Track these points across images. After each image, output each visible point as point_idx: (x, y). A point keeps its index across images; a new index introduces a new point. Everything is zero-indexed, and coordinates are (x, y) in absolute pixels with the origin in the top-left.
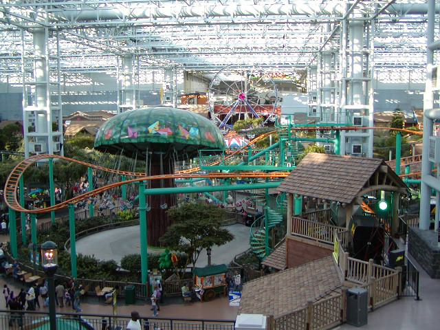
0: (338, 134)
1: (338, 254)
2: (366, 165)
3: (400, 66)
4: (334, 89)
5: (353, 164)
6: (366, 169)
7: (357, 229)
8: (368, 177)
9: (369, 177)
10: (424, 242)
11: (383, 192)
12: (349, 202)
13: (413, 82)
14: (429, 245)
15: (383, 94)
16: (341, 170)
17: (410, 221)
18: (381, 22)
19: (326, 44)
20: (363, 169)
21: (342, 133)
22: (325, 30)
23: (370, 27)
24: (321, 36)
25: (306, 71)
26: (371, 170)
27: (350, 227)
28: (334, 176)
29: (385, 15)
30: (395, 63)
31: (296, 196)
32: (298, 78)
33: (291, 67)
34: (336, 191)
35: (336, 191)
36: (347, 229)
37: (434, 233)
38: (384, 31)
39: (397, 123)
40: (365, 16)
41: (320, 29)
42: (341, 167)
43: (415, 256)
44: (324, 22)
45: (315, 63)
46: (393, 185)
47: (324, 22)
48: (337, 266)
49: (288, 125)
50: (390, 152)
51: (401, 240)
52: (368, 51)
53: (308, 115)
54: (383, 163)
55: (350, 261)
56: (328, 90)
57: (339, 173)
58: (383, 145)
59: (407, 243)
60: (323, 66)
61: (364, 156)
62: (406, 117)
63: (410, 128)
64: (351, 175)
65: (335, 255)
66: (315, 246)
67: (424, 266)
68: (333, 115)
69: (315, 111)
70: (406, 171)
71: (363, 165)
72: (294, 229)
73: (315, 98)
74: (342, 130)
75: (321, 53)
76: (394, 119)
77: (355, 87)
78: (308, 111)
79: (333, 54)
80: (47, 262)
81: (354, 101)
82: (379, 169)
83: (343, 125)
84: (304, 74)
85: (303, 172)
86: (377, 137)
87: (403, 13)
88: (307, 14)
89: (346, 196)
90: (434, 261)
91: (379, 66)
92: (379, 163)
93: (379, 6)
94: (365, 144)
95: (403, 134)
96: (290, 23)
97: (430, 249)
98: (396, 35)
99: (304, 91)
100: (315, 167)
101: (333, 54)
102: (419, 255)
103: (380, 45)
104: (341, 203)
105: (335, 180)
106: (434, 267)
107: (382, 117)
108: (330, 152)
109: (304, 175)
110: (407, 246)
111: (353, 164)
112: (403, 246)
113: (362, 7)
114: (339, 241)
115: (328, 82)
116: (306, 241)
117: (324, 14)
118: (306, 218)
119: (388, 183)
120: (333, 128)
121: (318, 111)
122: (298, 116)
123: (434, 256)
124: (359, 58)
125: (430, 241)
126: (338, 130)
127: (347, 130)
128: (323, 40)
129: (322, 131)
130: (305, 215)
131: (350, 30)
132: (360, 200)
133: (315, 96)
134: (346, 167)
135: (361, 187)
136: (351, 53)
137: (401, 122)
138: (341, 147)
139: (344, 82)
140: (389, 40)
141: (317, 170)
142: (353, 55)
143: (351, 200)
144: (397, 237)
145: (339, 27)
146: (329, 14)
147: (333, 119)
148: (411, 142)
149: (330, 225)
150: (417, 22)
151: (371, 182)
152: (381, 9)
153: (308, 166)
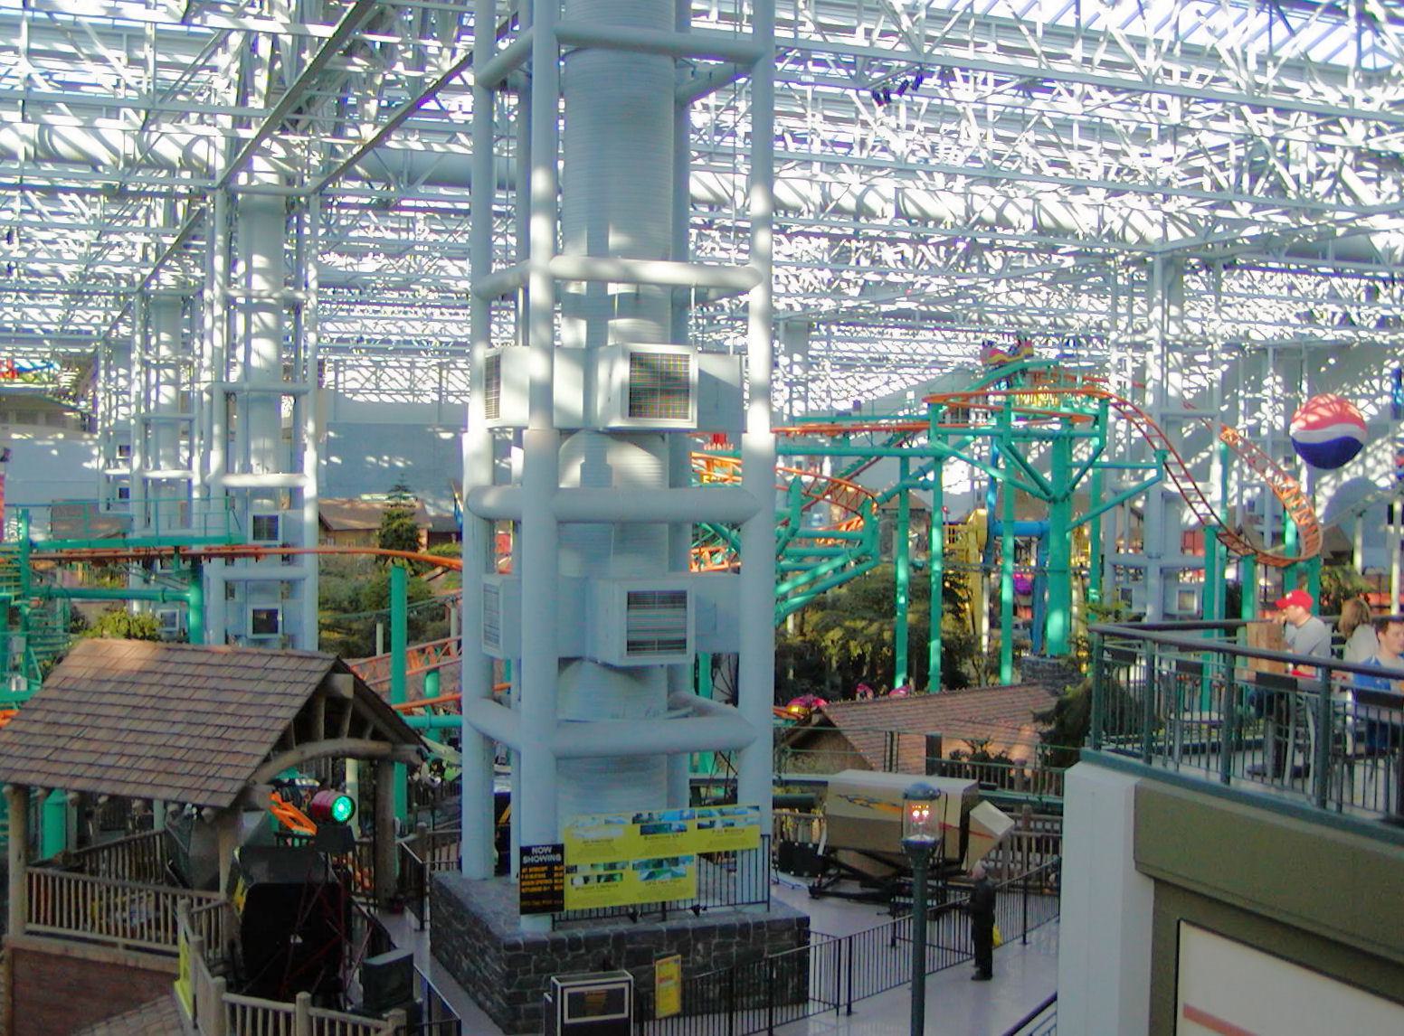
0: (196, 573)
1: (195, 987)
2: (284, 676)
3: (407, 348)
4: (191, 421)
5: (239, 673)
6: (281, 688)
7: (255, 894)
8: (288, 714)
9: (294, 712)
10: (477, 920)
11: (351, 766)
12: (225, 802)
13: (451, 399)
14: (496, 931)
15: (355, 434)
16: (199, 695)
17: (444, 850)
18: (341, 206)
19: (161, 265)
20: (272, 688)
21: (214, 571)
22: (158, 220)
23: (307, 218)
24: (147, 240)
25: (94, 358)
26: (299, 689)
27: (231, 889)
28: (171, 717)
29: (357, 184)
30: (394, 338)
31: (40, 792)
32: (66, 379)
33: (39, 341)
34: (180, 768)
35: (180, 768)
36: (221, 895)
37: (508, 884)
38: (353, 234)
39: (399, 536)
40: (290, 181)
41: (141, 213)
42: (199, 683)
43: (451, 967)
44: (153, 195)
45: (124, 330)
46: (376, 736)
47: (153, 195)
48: (189, 1027)
49: (20, 544)
50: (380, 629)
51: (410, 918)
52: (300, 295)
53: (102, 508)
54: (338, 667)
55: (233, 1007)
56: (171, 424)
57: (191, 706)
58: (355, 604)
59: (427, 926)
60: (153, 341)
61: (290, 640)
62: (432, 512)
63: (445, 547)
64: (230, 709)
65: (182, 989)
66: (114, 965)
67: (481, 997)
68: (187, 506)
69: (124, 493)
70: (430, 684)
71: (272, 676)
72: (33, 914)
73: (125, 450)
74: (209, 556)
75: (145, 296)
76: (391, 517)
77: (257, 414)
78: (101, 494)
79: (186, 302)
80: (916, 831)
81: (253, 461)
82: (324, 687)
83: (216, 540)
84: (87, 368)
85: (62, 707)
86: (335, 581)
87: (412, 181)
88: (93, 163)
89: (213, 785)
90: (509, 977)
91: (341, 346)
92: (326, 666)
93: (332, 150)
94: (290, 604)
95: (418, 567)
96: (33, 189)
97: (495, 940)
98: (394, 250)
99: (87, 424)
100: (107, 687)
101: (185, 299)
102: (465, 963)
103: (341, 279)
104: (200, 808)
105: (177, 728)
106: (508, 998)
107: (355, 513)
108: (175, 637)
109: (66, 719)
110: (427, 934)
111: (239, 673)
112: (410, 939)
113: (279, 152)
114: (194, 938)
115: (167, 394)
116: (78, 951)
117: (150, 165)
118: (80, 870)
119: (356, 732)
120: (178, 553)
121: (135, 494)
122: (61, 512)
123: (510, 962)
124: (268, 318)
125: (497, 914)
126: (196, 560)
127: (230, 558)
128: (152, 257)
129: (147, 562)
130: (80, 858)
131: (241, 226)
132: (264, 795)
133: (125, 443)
134: (213, 683)
135: (264, 750)
136: (241, 300)
137: (413, 530)
138: (210, 614)
139: (219, 397)
140: (369, 265)
141: (113, 699)
142: (249, 309)
143: (232, 797)
144: (394, 907)
145: (202, 211)
146: (170, 167)
147: (186, 522)
148: (445, 593)
149: (164, 888)
150: (458, 212)
151: (301, 729)
152: (342, 161)
153: (83, 686)
